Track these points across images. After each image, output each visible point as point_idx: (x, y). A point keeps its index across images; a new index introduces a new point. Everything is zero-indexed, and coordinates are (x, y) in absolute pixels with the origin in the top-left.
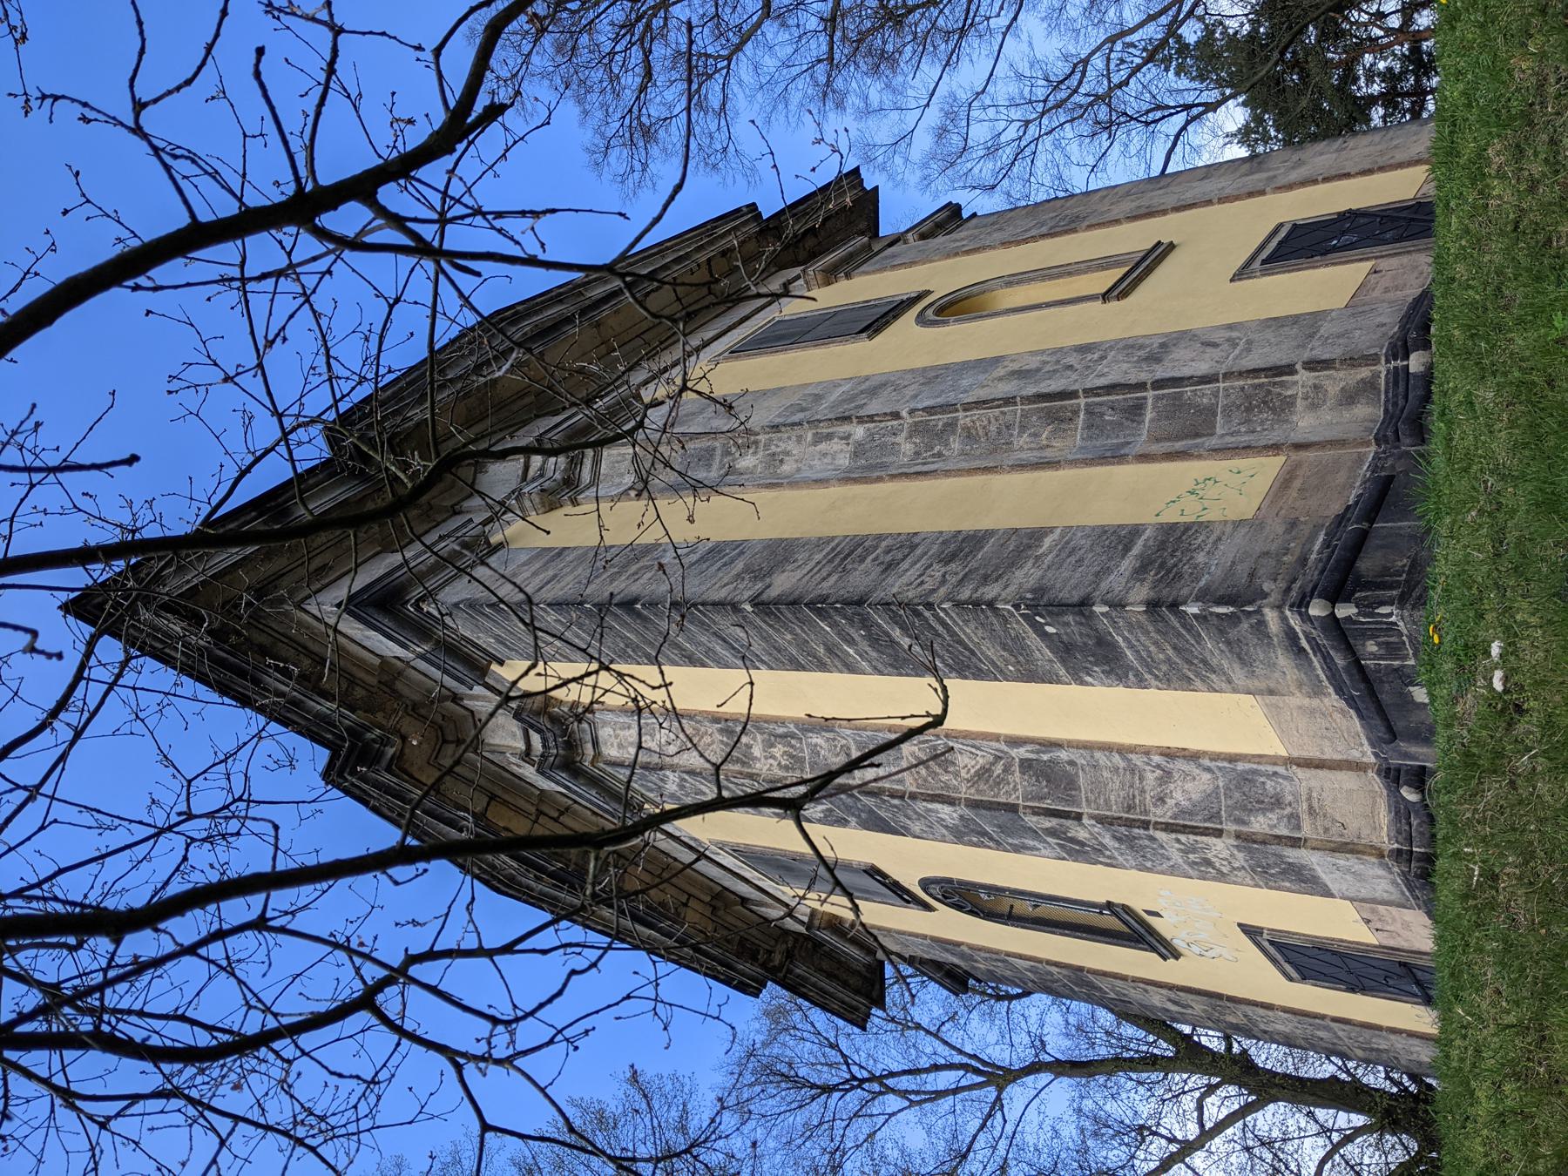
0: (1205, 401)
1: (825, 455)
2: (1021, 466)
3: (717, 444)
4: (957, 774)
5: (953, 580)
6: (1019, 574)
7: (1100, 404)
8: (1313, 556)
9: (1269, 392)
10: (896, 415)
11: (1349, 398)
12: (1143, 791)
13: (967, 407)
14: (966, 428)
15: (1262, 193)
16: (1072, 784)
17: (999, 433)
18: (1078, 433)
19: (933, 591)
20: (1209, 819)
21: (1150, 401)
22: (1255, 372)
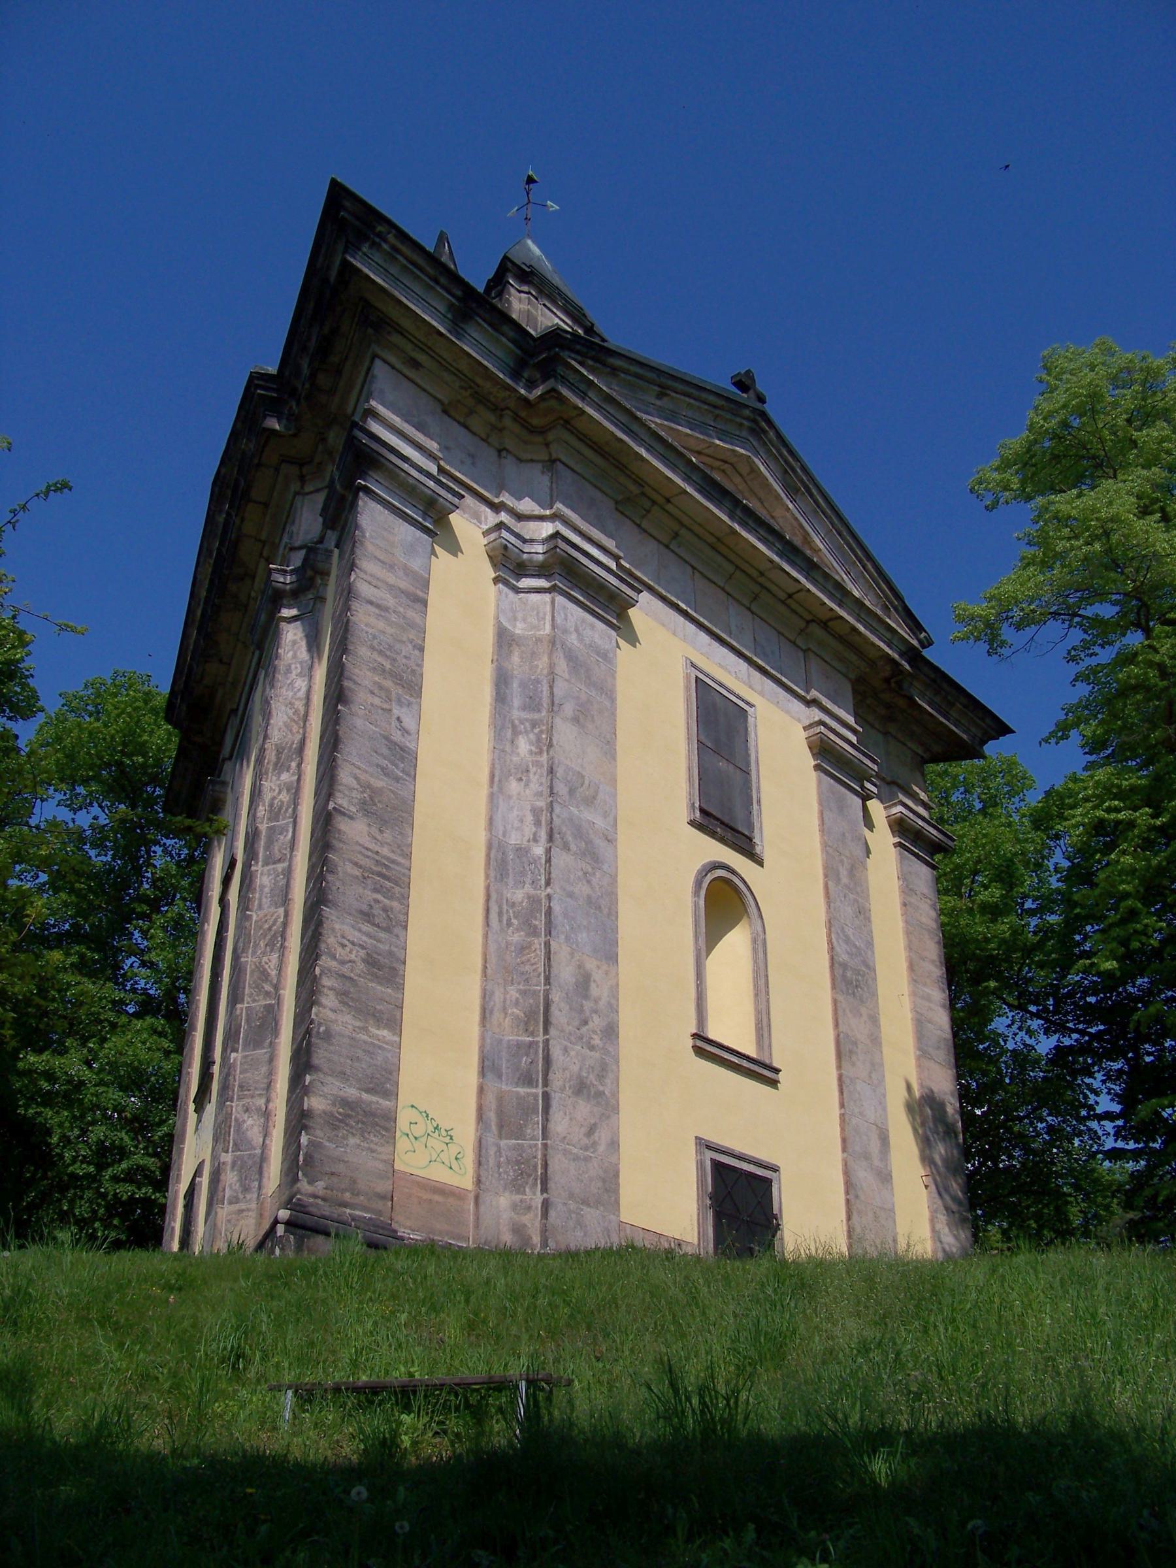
0: (529, 1131)
1: (521, 821)
2: (485, 995)
3: (544, 713)
4: (264, 954)
5: (345, 969)
6: (348, 1018)
7: (536, 1052)
8: (348, 1211)
9: (529, 1176)
10: (548, 883)
11: (518, 1230)
12: (252, 1097)
13: (547, 944)
14: (530, 944)
15: (844, 1150)
16: (258, 1044)
17: (522, 973)
18: (512, 1036)
19: (334, 957)
20: (235, 1144)
21: (534, 1090)
22: (545, 1166)
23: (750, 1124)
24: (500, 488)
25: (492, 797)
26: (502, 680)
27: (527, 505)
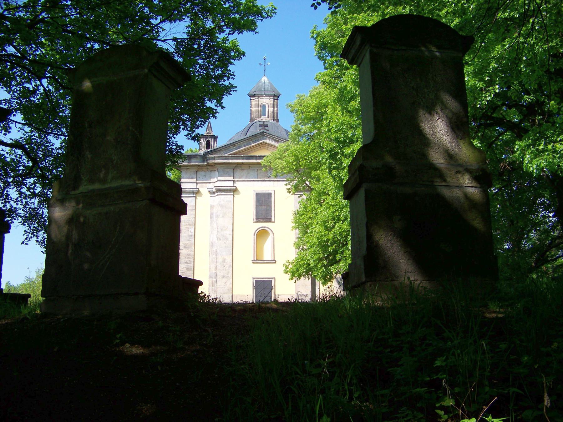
2: (210, 266)
23: (264, 272)
24: (211, 177)
25: (210, 236)
26: (212, 214)
27: (215, 180)
